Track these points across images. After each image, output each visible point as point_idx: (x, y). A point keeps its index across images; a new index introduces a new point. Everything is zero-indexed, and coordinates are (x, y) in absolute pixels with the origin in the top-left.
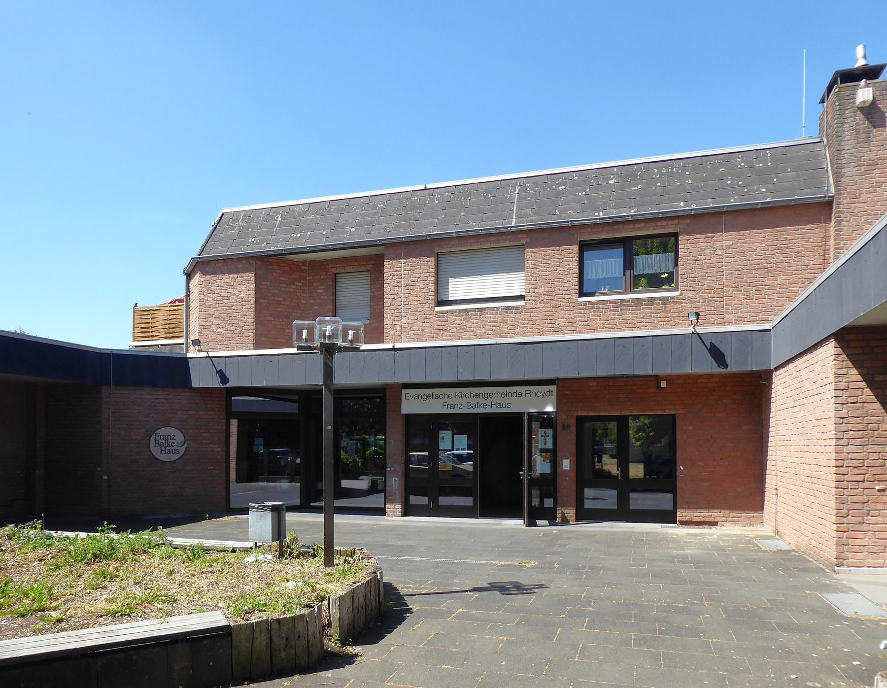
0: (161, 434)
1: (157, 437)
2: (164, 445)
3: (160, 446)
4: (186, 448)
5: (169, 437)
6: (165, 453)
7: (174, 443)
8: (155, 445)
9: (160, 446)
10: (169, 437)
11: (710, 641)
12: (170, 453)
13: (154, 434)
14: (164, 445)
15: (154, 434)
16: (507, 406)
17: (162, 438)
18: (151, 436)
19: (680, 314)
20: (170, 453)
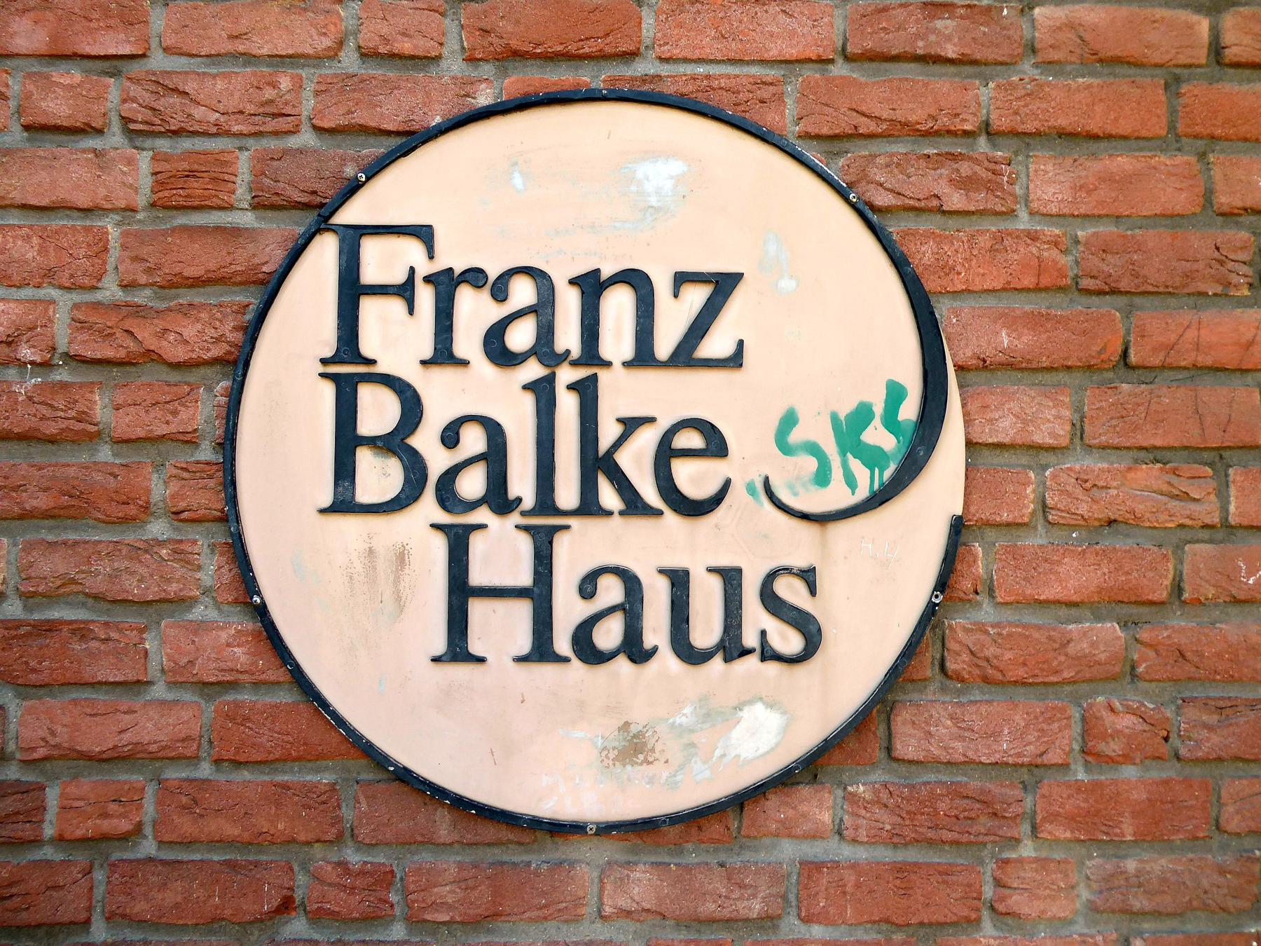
0: (453, 257)
1: (370, 309)
2: (522, 484)
3: (428, 508)
4: (958, 527)
5: (705, 632)
6: (542, 651)
7: (716, 445)
8: (344, 470)
9: (428, 508)
10: (705, 632)
11: (1081, 775)
12: (634, 648)
13: (325, 252)
14: (522, 484)
15: (325, 252)
16: (756, 619)
17: (468, 342)
18: (272, 286)
19: (129, 800)
20: (634, 648)
